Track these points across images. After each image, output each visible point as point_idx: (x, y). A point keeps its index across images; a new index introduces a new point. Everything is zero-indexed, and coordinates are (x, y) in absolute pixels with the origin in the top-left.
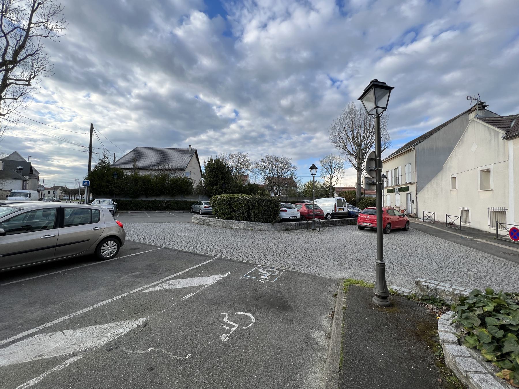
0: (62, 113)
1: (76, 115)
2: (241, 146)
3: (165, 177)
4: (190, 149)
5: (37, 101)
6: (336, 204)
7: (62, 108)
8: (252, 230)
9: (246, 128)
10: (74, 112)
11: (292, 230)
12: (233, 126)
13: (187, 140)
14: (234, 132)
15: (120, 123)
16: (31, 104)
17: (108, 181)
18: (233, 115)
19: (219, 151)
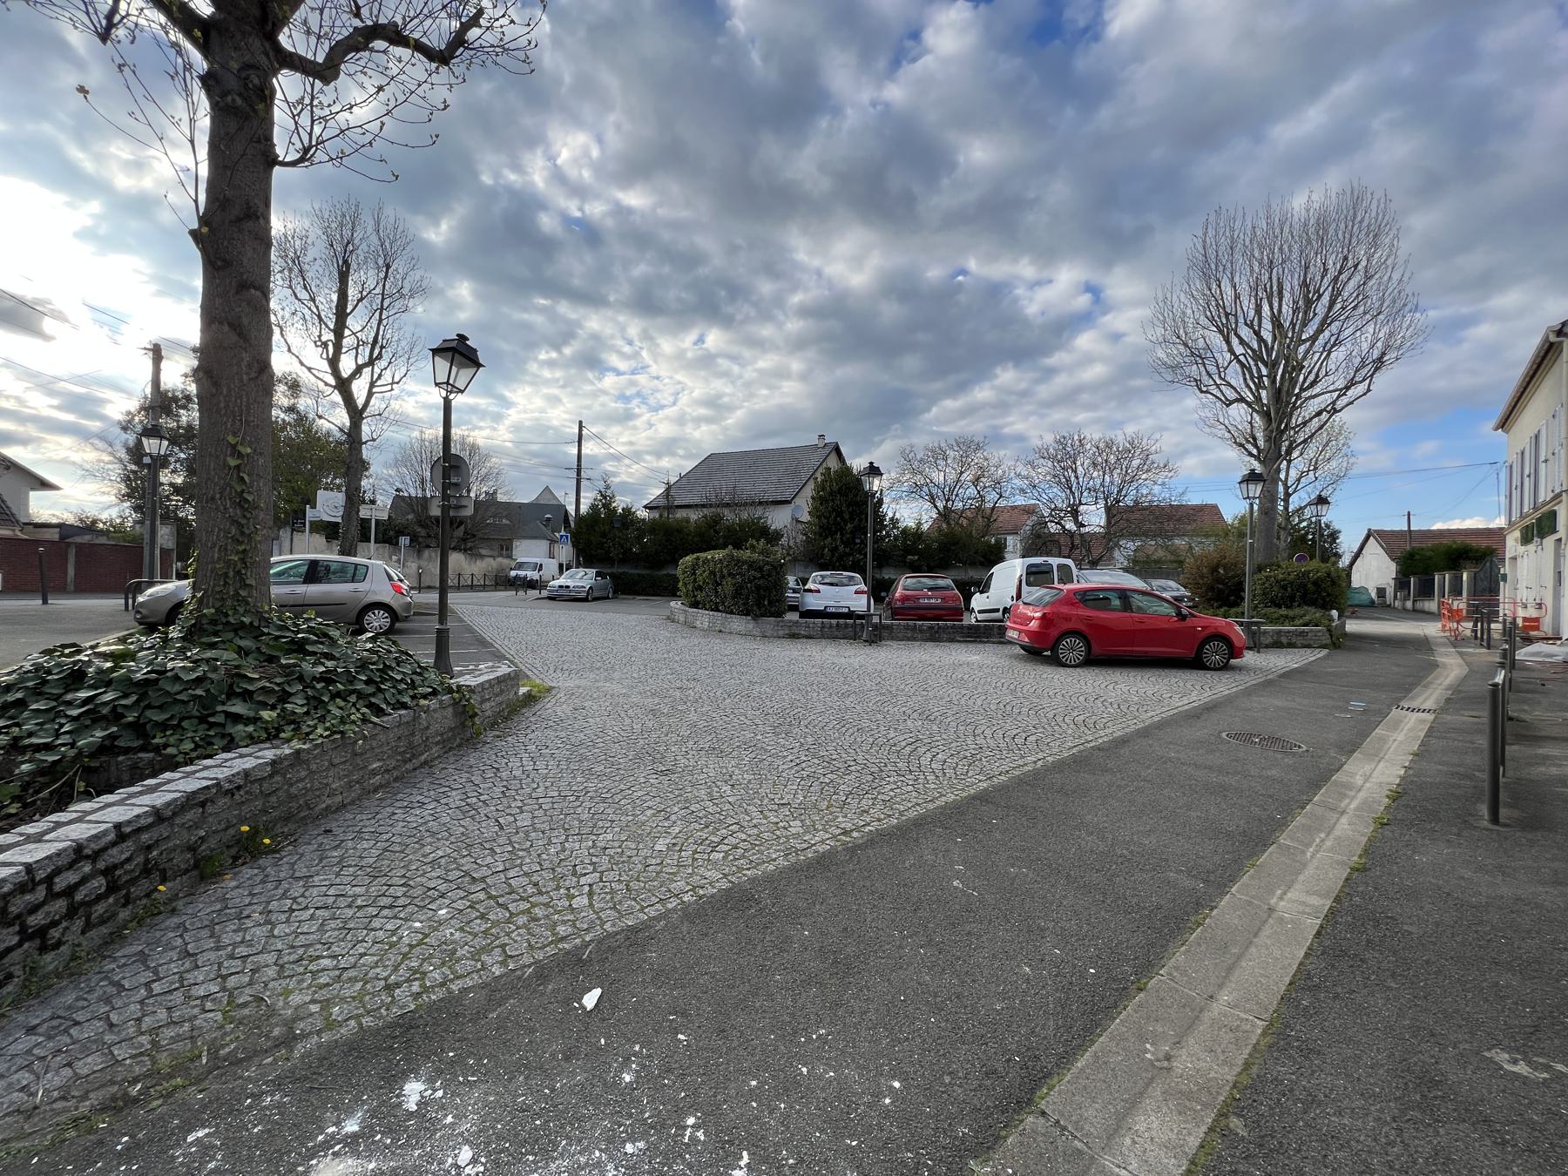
0: (658, 391)
1: (683, 390)
2: (1113, 404)
5: (618, 373)
7: (658, 378)
10: (679, 383)
11: (809, 637)
12: (1085, 341)
13: (934, 410)
14: (1088, 360)
15: (765, 392)
16: (609, 381)
17: (604, 535)
18: (1084, 301)
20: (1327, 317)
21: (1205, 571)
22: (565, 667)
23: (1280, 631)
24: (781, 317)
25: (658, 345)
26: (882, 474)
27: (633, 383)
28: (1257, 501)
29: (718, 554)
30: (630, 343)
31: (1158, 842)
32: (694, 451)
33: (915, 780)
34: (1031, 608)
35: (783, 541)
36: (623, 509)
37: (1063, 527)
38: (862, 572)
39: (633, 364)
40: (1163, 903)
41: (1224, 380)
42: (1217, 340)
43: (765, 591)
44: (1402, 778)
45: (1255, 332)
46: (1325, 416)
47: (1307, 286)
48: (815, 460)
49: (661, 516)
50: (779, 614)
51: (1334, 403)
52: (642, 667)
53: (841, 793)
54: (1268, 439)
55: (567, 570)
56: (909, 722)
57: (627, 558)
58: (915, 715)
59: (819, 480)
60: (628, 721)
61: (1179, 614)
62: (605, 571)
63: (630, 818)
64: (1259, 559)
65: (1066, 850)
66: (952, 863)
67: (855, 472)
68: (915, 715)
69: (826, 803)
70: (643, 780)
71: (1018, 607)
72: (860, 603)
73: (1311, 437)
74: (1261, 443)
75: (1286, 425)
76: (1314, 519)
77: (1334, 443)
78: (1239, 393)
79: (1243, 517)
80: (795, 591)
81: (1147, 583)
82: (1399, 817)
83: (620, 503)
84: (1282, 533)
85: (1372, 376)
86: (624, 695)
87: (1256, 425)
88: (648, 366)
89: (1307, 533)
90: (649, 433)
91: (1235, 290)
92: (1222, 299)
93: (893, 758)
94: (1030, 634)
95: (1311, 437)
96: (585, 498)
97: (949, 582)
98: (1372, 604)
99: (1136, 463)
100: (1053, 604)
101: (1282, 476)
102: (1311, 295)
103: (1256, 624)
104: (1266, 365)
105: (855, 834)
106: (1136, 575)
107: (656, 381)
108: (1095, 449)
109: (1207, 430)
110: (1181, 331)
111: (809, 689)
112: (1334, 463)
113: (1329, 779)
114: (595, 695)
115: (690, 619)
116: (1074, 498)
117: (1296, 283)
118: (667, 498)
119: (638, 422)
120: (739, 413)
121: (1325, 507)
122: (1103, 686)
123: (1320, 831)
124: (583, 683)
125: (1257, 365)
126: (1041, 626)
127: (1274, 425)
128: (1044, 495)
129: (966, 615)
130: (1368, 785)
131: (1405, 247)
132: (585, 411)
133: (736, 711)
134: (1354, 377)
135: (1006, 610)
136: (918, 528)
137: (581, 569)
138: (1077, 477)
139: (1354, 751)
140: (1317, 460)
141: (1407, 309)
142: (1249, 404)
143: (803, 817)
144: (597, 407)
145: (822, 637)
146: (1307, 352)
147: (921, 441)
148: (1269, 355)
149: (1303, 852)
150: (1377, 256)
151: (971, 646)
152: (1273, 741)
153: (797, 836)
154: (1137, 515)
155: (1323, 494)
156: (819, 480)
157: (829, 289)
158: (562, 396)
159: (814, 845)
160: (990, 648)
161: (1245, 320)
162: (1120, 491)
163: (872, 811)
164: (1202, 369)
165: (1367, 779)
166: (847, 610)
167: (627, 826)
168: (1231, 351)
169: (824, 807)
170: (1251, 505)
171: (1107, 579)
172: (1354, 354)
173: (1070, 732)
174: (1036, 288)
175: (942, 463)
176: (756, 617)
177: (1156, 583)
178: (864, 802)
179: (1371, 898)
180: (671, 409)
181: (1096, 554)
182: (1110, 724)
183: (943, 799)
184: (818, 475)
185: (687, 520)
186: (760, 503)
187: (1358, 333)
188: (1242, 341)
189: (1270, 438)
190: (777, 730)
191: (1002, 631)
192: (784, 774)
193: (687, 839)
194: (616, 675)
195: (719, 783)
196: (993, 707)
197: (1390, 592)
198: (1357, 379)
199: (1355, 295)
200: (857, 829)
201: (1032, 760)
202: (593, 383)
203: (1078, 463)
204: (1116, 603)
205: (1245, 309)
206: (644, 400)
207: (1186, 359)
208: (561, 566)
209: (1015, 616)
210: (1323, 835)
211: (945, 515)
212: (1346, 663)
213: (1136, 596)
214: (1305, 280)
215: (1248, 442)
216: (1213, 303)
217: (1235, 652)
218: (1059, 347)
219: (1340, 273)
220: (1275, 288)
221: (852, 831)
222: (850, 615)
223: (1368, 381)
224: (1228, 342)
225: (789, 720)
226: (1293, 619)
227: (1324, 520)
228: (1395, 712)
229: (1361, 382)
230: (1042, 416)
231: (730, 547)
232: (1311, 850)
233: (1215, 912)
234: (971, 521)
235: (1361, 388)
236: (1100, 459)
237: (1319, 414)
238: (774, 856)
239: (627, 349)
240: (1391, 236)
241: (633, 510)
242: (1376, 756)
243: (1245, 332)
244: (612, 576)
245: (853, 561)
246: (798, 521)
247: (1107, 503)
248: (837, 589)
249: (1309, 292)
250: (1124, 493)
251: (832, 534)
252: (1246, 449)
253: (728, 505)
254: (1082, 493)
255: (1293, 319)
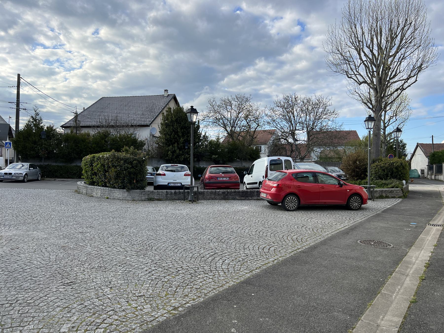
0: (70, 59)
1: (86, 60)
2: (311, 81)
3: (106, 135)
4: (166, 95)
5: (45, 47)
6: (269, 167)
7: (70, 52)
8: (108, 198)
9: (318, 50)
10: (84, 56)
11: (159, 200)
12: (298, 49)
13: (226, 79)
14: (299, 58)
15: (135, 64)
16: (39, 51)
17: (35, 143)
18: (297, 29)
19: (274, 94)
20: (399, 46)
21: (351, 163)
22: (7, 223)
23: (382, 191)
24: (144, 24)
25: (70, 33)
26: (197, 113)
27: (55, 54)
28: (372, 130)
29: (106, 155)
30: (52, 30)
31: (329, 297)
32: (93, 95)
33: (213, 276)
34: (272, 182)
35: (145, 147)
36: (47, 128)
37: (288, 141)
38: (188, 164)
39: (55, 42)
40: (331, 328)
41: (358, 72)
42: (355, 53)
43: (134, 175)
44: (430, 257)
45: (370, 50)
46: (399, 91)
47: (392, 31)
48: (162, 103)
49: (72, 132)
50: (142, 188)
51: (403, 85)
52: (58, 221)
53: (174, 287)
54: (376, 101)
55: (10, 163)
56: (211, 244)
57: (50, 156)
58: (215, 240)
59: (165, 114)
60: (47, 254)
61: (339, 184)
62: (36, 164)
63: (45, 314)
64: (373, 157)
65: (287, 306)
66: (231, 319)
67: (185, 110)
68: (215, 240)
69: (165, 293)
70: (55, 290)
71: (265, 181)
72: (187, 181)
73: (394, 100)
74: (373, 102)
75: (384, 95)
76: (396, 138)
77: (403, 103)
78: (364, 79)
79: (367, 137)
80: (152, 174)
81: (326, 169)
82: (429, 275)
83: (46, 124)
84: (383, 145)
85: (417, 74)
86: (46, 239)
87: (372, 94)
88: (64, 45)
89: (393, 145)
90: (66, 83)
91: (362, 30)
92: (357, 34)
93: (202, 264)
94: (271, 195)
95: (394, 100)
96: (23, 120)
97: (232, 169)
98: (419, 177)
99: (321, 110)
100: (282, 180)
101: (383, 118)
102: (393, 35)
103: (373, 187)
104: (375, 66)
105: (180, 309)
106: (321, 165)
107: (69, 54)
108: (302, 103)
109: (351, 96)
110: (340, 48)
111: (158, 229)
112: (403, 113)
113: (402, 260)
114: (26, 240)
115: (89, 191)
116: (293, 127)
117: (387, 29)
118: (76, 121)
119: (58, 77)
120: (120, 75)
121: (400, 133)
122: (306, 220)
123: (398, 285)
124: (18, 232)
125: (371, 66)
126: (276, 191)
127: (379, 95)
128: (279, 125)
129: (241, 185)
130: (417, 261)
131: (429, 17)
132: (23, 68)
133: (115, 244)
134: (410, 74)
135: (260, 183)
136: (218, 141)
137: (20, 163)
138: (294, 117)
139: (412, 246)
140: (397, 111)
141: (430, 45)
142: (368, 84)
143: (152, 302)
144: (31, 67)
145: (167, 199)
146: (392, 61)
147: (219, 96)
148: (377, 62)
149: (391, 296)
150: (419, 20)
151: (244, 202)
152: (380, 243)
153: (147, 314)
154: (321, 135)
155: (399, 127)
156: (165, 114)
157: (171, 11)
158: (8, 58)
159: (157, 317)
160: (253, 203)
161: (367, 45)
162: (313, 124)
163: (190, 295)
164: (348, 66)
165: (417, 258)
166: (180, 185)
167: (43, 319)
168: (361, 59)
169: (164, 295)
170: (370, 132)
171: (307, 167)
172: (410, 63)
173: (290, 244)
174: (275, 21)
175: (229, 107)
176: (129, 190)
177: (330, 168)
178: (186, 290)
179: (418, 315)
180: (78, 70)
181: (303, 154)
182: (308, 239)
183: (228, 285)
184: (164, 111)
185: (88, 135)
186: (132, 126)
187: (412, 54)
188: (365, 55)
189: (377, 100)
190: (139, 253)
191: (259, 193)
192: (142, 279)
193: (81, 323)
194: (41, 226)
195: (103, 287)
196: (254, 233)
197: (426, 171)
198: (412, 75)
199: (410, 37)
200: (182, 306)
201: (271, 261)
202: (28, 52)
203: (295, 110)
204: (311, 178)
205: (367, 39)
206: (62, 64)
207: (342, 61)
208: (6, 161)
209: (264, 185)
210: (399, 287)
211: (231, 134)
212: (409, 205)
213: (320, 175)
214: (391, 28)
215: (368, 102)
216: (353, 35)
217: (363, 201)
218: (286, 51)
219: (404, 26)
220: (379, 31)
221: (178, 307)
222: (182, 187)
223: (416, 76)
224: (359, 54)
225: (146, 247)
226: (387, 185)
227: (399, 139)
228: (428, 227)
229: (413, 77)
230: (278, 85)
231: (113, 150)
232: (395, 294)
233: (354, 330)
234: (244, 138)
235: (413, 79)
236: (304, 108)
237: (397, 90)
238: (134, 327)
239: (50, 33)
240: (424, 12)
241: (54, 128)
242: (420, 248)
243: (366, 50)
244: (40, 167)
245: (184, 158)
246: (154, 136)
247: (308, 129)
248: (175, 173)
249: (392, 34)
250: (315, 125)
251: (173, 144)
252: (367, 106)
253: (113, 127)
254: (296, 125)
255: (386, 46)
